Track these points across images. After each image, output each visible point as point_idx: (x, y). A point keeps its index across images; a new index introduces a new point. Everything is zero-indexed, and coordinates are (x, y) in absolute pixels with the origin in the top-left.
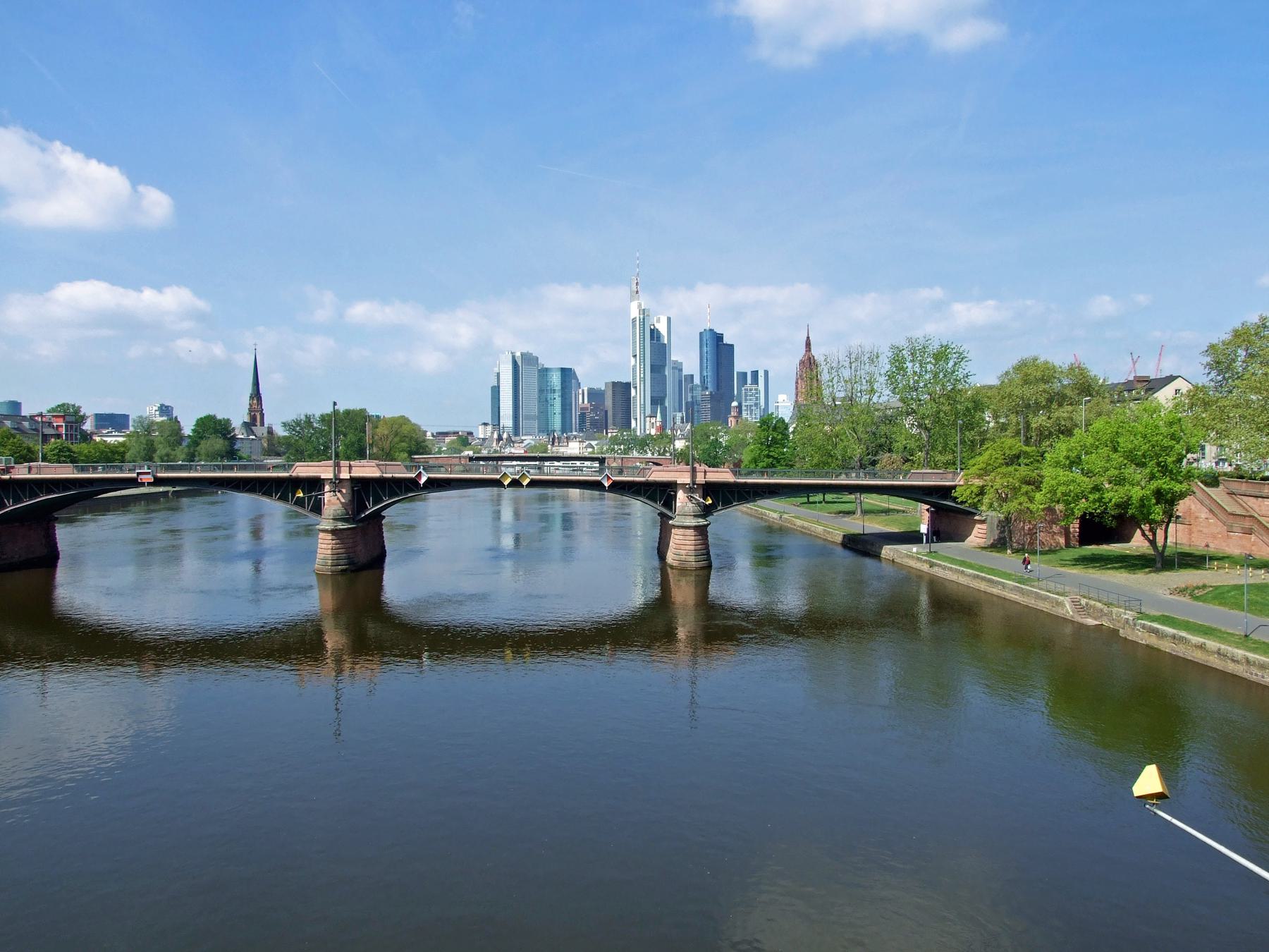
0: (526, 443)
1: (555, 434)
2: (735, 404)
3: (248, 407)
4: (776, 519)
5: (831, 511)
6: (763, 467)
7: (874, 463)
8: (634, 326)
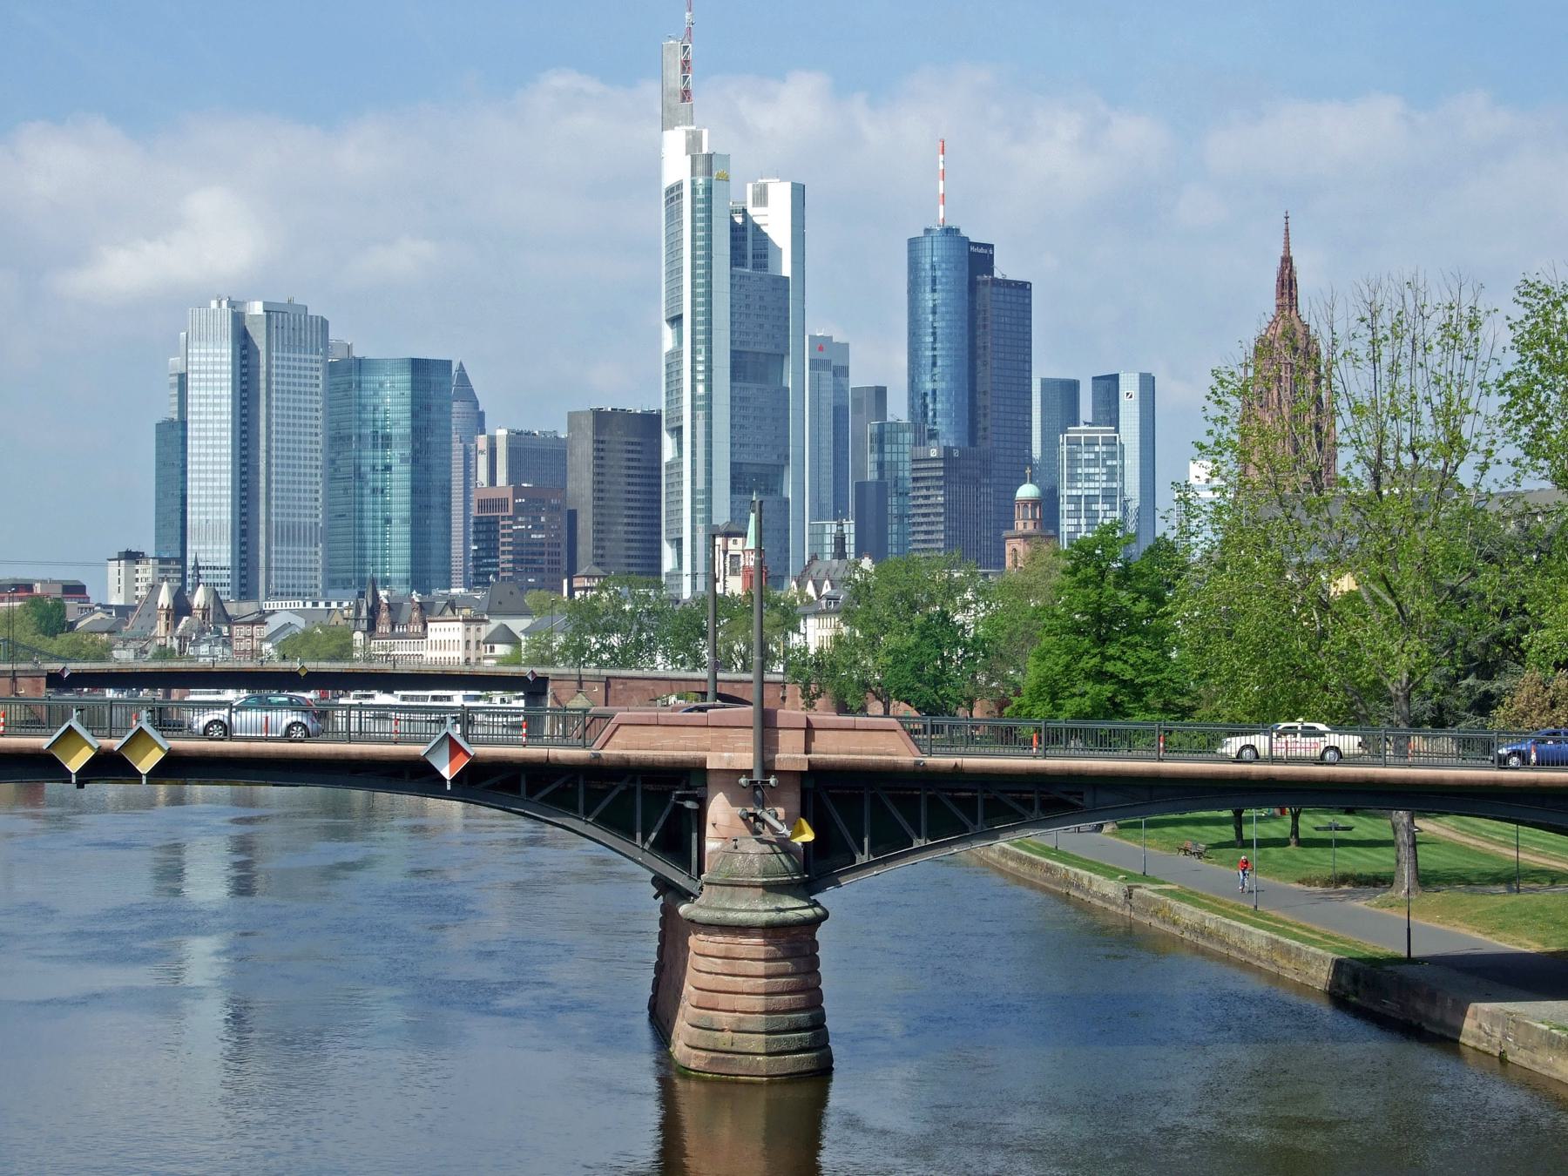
0: (274, 623)
1: (383, 594)
2: (1027, 491)
4: (1112, 901)
5: (1314, 873)
6: (1080, 715)
7: (1485, 705)
8: (673, 216)
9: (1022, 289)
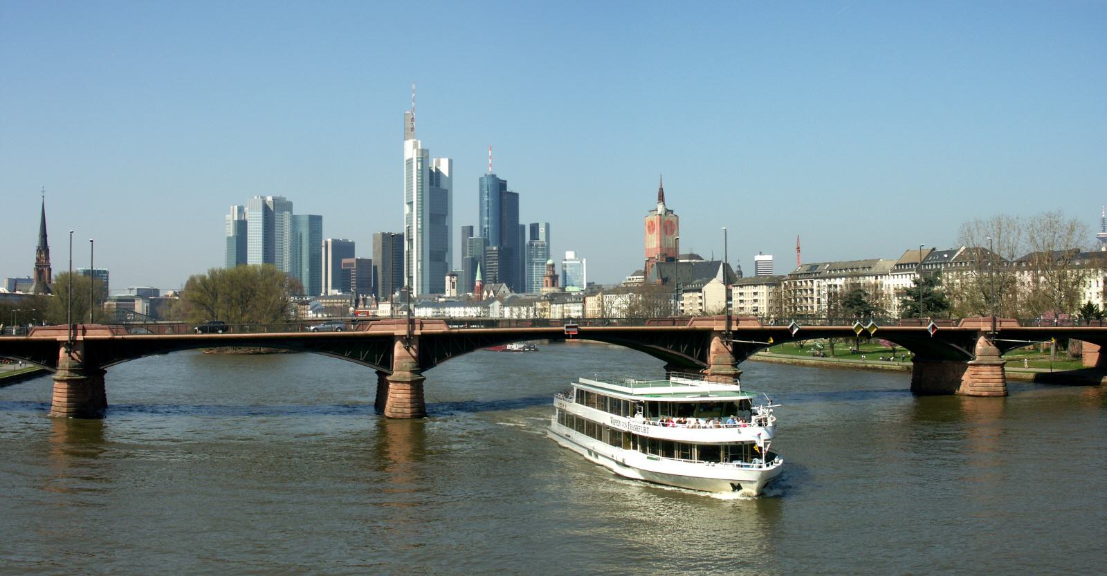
3: (35, 261)
9: (516, 195)
